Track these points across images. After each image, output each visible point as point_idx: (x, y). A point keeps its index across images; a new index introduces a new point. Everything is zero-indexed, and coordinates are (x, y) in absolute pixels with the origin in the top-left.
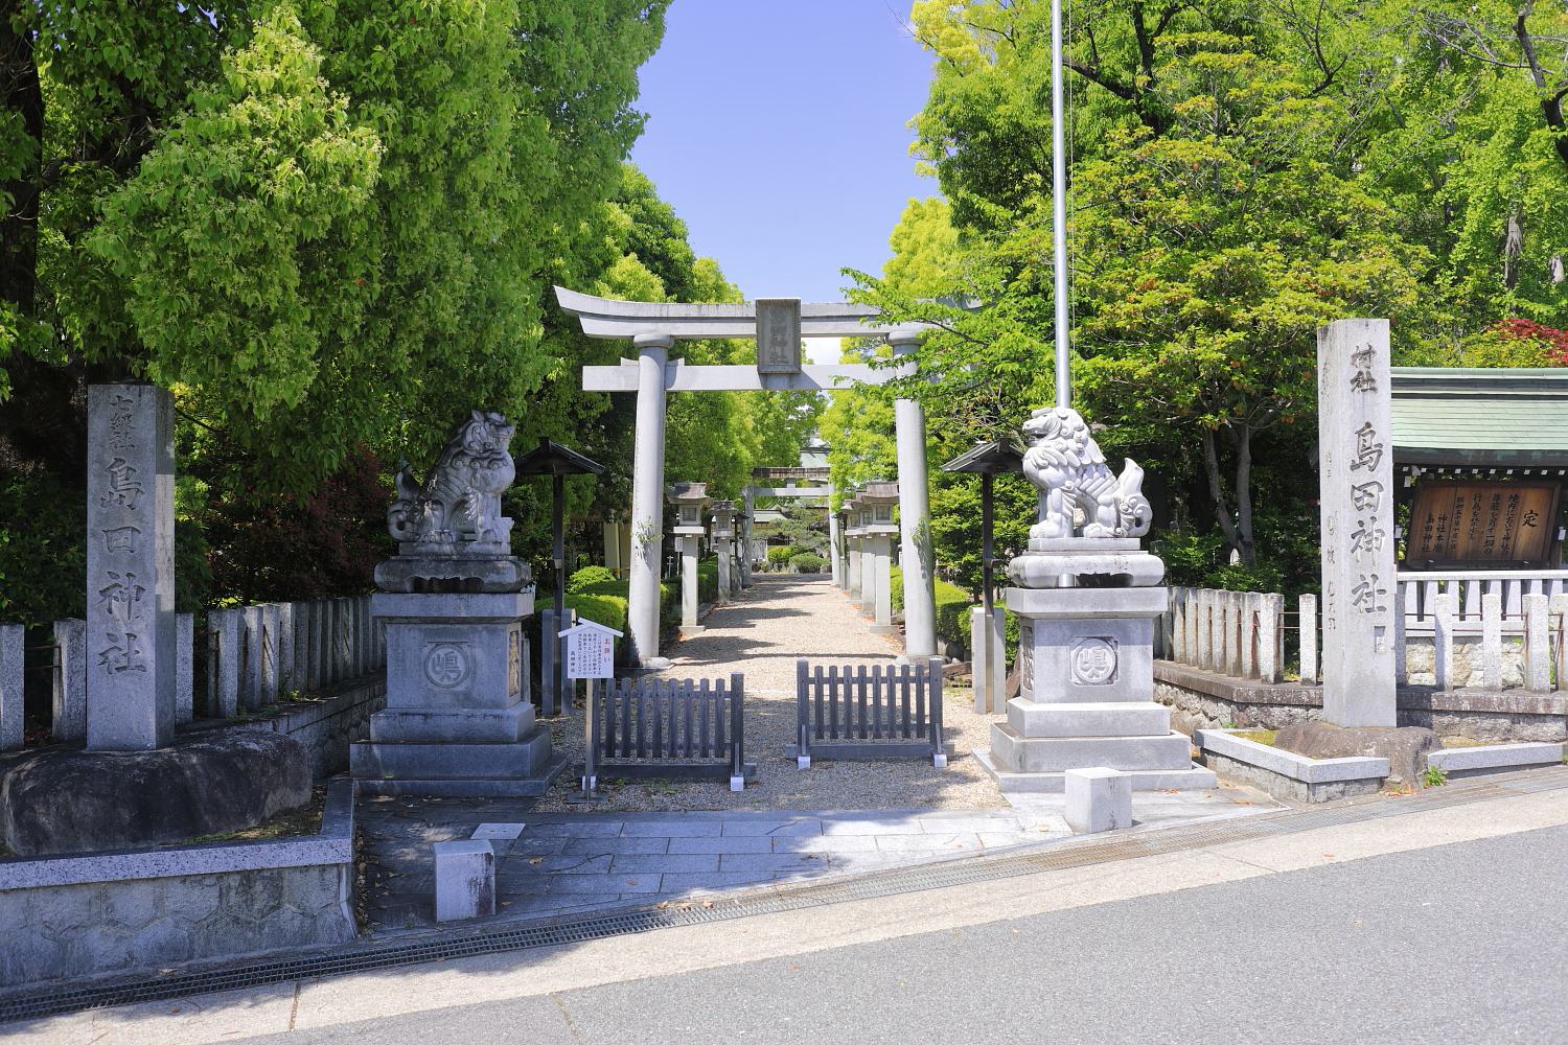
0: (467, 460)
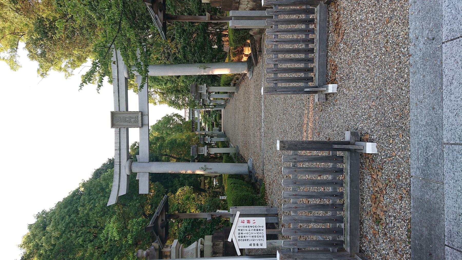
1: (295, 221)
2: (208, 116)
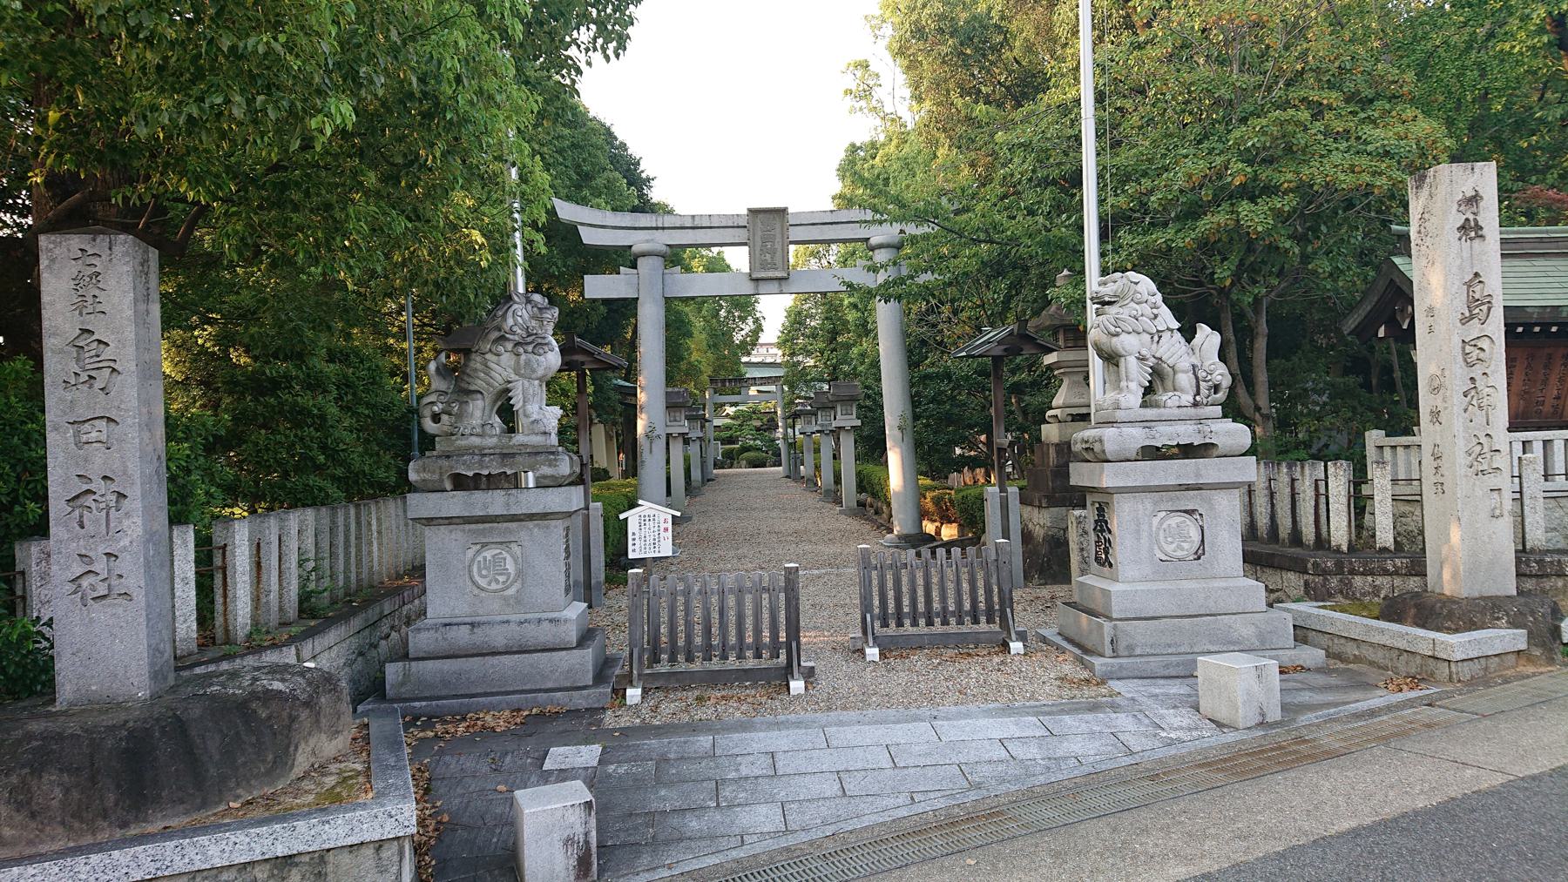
0: (509, 346)
1: (687, 593)
2: (758, 423)
